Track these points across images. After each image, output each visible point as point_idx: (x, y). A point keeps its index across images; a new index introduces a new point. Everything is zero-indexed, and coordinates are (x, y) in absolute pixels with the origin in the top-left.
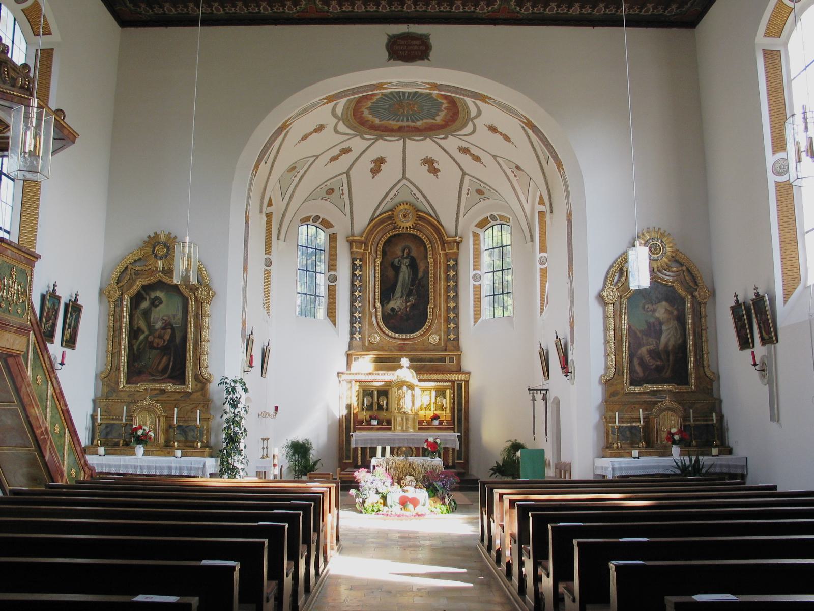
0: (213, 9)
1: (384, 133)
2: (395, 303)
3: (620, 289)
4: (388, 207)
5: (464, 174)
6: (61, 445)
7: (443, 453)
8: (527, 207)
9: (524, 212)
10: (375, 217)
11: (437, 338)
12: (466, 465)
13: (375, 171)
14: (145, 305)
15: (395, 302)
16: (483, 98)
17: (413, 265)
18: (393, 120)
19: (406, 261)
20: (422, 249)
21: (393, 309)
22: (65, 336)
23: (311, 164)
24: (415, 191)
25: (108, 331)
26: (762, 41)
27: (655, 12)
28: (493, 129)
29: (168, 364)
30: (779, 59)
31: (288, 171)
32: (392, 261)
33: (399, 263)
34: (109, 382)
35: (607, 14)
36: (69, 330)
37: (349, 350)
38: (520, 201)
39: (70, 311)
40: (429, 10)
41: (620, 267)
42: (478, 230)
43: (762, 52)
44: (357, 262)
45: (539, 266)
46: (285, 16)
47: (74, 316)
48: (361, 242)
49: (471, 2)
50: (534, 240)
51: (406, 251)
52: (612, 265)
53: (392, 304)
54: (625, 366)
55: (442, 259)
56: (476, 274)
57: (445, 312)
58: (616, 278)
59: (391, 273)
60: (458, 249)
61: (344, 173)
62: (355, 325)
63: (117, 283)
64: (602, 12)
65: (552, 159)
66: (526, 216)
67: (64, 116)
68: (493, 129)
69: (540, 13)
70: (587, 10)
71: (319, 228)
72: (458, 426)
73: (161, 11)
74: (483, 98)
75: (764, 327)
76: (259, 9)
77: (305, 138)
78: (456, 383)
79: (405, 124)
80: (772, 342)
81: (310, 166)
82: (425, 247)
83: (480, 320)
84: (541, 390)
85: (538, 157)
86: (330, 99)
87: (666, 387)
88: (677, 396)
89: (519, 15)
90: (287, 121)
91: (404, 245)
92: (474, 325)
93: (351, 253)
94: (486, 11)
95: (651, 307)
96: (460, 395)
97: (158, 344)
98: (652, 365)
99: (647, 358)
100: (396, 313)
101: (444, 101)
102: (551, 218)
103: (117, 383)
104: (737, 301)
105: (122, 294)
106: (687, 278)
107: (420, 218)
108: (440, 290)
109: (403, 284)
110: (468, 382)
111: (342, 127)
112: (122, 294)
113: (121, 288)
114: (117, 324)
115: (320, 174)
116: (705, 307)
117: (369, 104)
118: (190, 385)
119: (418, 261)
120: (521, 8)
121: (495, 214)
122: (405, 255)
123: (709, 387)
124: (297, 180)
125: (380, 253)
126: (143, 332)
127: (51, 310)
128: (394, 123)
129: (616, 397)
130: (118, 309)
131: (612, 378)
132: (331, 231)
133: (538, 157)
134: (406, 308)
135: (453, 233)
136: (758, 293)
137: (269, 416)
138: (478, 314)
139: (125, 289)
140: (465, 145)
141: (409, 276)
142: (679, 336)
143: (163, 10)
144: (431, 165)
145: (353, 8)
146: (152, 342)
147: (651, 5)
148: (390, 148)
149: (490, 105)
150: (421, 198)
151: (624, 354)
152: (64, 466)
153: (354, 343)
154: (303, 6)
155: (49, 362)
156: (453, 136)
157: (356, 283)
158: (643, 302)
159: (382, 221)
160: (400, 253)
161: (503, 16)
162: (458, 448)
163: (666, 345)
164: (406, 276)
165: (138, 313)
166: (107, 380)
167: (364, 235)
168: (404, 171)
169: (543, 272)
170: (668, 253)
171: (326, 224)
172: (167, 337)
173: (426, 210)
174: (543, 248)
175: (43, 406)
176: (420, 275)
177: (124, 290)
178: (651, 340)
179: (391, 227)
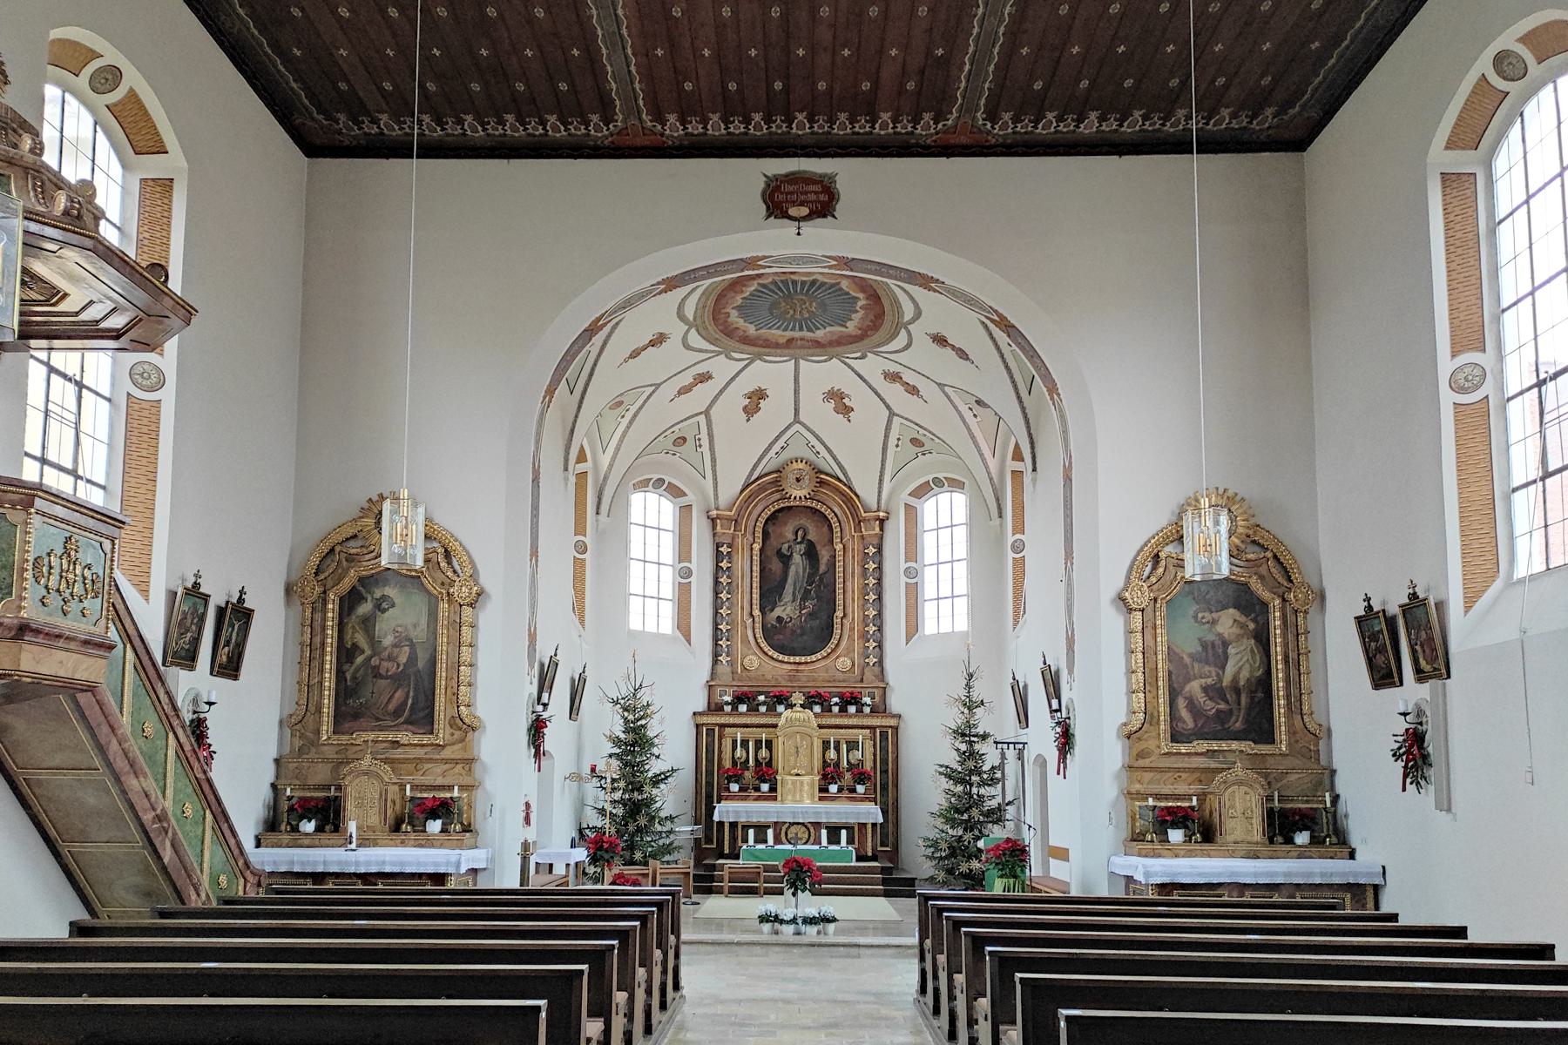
0: (466, 127)
1: (764, 350)
3: (1155, 587)
5: (892, 414)
6: (196, 836)
7: (856, 831)
8: (993, 464)
9: (989, 473)
11: (849, 663)
12: (894, 855)
13: (751, 410)
14: (365, 608)
16: (926, 282)
17: (811, 554)
18: (778, 328)
20: (825, 529)
21: (779, 619)
22: (218, 658)
23: (648, 398)
24: (814, 442)
25: (302, 651)
26: (1440, 158)
27: (1234, 125)
28: (940, 340)
29: (405, 702)
30: (1473, 189)
31: (610, 408)
34: (303, 731)
35: (1147, 131)
36: (226, 649)
37: (712, 679)
39: (227, 618)
40: (835, 131)
41: (1155, 551)
42: (912, 501)
43: (1439, 177)
44: (724, 549)
45: (1011, 555)
46: (592, 143)
47: (236, 627)
48: (729, 519)
49: (908, 115)
50: (1003, 514)
52: (1141, 550)
53: (778, 612)
54: (1161, 709)
58: (1148, 570)
59: (776, 566)
60: (882, 529)
61: (701, 413)
62: (720, 642)
63: (316, 574)
64: (1137, 128)
65: (1039, 380)
66: (991, 479)
67: (167, 277)
68: (940, 340)
69: (1026, 133)
70: (1111, 125)
72: (882, 795)
73: (375, 130)
74: (926, 282)
75: (1424, 651)
77: (635, 354)
78: (878, 731)
79: (797, 334)
80: (1439, 677)
81: (645, 402)
84: (1014, 743)
85: (1014, 382)
86: (671, 284)
87: (1235, 745)
88: (1257, 763)
89: (990, 138)
90: (598, 319)
93: (714, 535)
94: (932, 131)
95: (1208, 616)
96: (884, 749)
97: (387, 671)
98: (1210, 710)
99: (1201, 698)
100: (785, 627)
101: (861, 296)
102: (1034, 481)
103: (318, 732)
104: (1370, 607)
105: (325, 592)
106: (1273, 570)
107: (822, 483)
108: (853, 591)
109: (795, 584)
111: (695, 339)
112: (325, 592)
113: (323, 583)
114: (317, 640)
115: (666, 411)
116: (1305, 618)
117: (739, 300)
118: (443, 732)
119: (818, 548)
120: (994, 123)
121: (941, 476)
122: (799, 540)
123: (1312, 747)
124: (625, 422)
125: (759, 534)
126: (363, 652)
127: (189, 617)
128: (779, 332)
129: (1148, 761)
130: (318, 616)
131: (1140, 729)
132: (683, 501)
133: (1014, 382)
134: (800, 616)
136: (1415, 593)
139: (330, 583)
140: (894, 368)
142: (1258, 664)
143: (379, 127)
144: (838, 399)
145: (705, 128)
146: (377, 668)
147: (1228, 110)
148: (772, 373)
149: (937, 294)
150: (824, 452)
151: (1161, 692)
152: (202, 871)
153: (719, 668)
155: (167, 700)
156: (874, 353)
157: (722, 580)
158: (1195, 607)
159: (762, 489)
160: (790, 536)
161: (964, 140)
162: (881, 820)
163: (1235, 679)
164: (801, 571)
165: (353, 621)
166: (298, 726)
168: (797, 411)
169: (1020, 565)
170: (1240, 530)
171: (675, 492)
172: (403, 659)
173: (830, 471)
175: (158, 773)
176: (822, 568)
177: (329, 586)
178: (1207, 668)
179: (777, 496)
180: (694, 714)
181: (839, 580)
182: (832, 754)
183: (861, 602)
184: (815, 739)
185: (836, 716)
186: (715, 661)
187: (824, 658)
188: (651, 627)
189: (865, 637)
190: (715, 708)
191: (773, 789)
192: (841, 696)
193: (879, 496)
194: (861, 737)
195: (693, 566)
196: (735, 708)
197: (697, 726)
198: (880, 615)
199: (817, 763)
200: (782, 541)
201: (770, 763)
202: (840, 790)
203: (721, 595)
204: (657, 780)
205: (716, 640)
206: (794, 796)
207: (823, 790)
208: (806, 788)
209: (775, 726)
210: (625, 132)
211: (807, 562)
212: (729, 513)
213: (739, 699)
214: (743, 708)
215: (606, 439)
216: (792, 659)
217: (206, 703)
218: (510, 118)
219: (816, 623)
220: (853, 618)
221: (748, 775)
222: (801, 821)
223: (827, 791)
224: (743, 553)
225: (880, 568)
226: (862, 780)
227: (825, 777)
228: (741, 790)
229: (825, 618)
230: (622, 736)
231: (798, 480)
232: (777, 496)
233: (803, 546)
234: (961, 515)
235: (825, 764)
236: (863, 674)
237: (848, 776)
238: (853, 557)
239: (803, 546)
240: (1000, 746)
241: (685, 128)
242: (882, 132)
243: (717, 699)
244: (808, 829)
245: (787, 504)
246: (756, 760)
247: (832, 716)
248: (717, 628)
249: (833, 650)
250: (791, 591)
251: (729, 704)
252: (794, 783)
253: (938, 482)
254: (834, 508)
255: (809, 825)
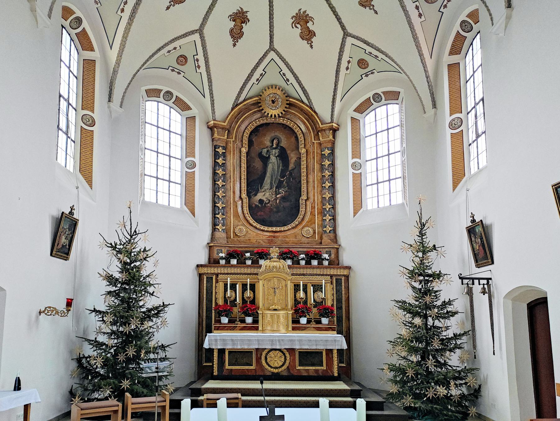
2: (264, 195)
4: (256, 90)
9: (426, 71)
10: (239, 102)
15: (264, 193)
17: (283, 156)
19: (276, 152)
20: (293, 139)
21: (261, 201)
24: (285, 70)
32: (260, 151)
33: (267, 154)
38: (421, 55)
42: (357, 115)
44: (220, 150)
48: (223, 128)
51: (275, 141)
53: (260, 196)
55: (316, 150)
56: (355, 162)
57: (319, 204)
59: (258, 164)
60: (334, 137)
71: (173, 108)
78: (334, 278)
82: (297, 137)
83: (361, 210)
84: (479, 279)
91: (273, 135)
92: (354, 216)
93: (213, 140)
96: (338, 292)
100: (265, 206)
107: (291, 105)
108: (314, 182)
109: (272, 177)
110: (348, 277)
119: (288, 152)
122: (274, 146)
134: (276, 199)
135: (328, 119)
137: (57, 313)
138: (358, 204)
141: (278, 167)
150: (292, 80)
153: (218, 234)
159: (247, 109)
160: (268, 143)
162: (345, 347)
167: (227, 121)
171: (182, 105)
176: (291, 166)
180: (198, 266)
181: (304, 174)
182: (301, 294)
183: (320, 189)
184: (289, 282)
185: (303, 267)
186: (214, 229)
187: (293, 228)
188: (163, 200)
189: (322, 213)
190: (213, 262)
191: (256, 321)
192: (307, 254)
193: (333, 111)
194: (324, 281)
195: (197, 160)
196: (228, 262)
197: (200, 276)
198: (333, 197)
199: (290, 302)
200: (262, 147)
201: (253, 302)
202: (309, 322)
203: (218, 183)
204: (150, 314)
205: (214, 214)
206: (272, 326)
207: (296, 321)
208: (282, 319)
209: (257, 274)
211: (280, 162)
212: (223, 124)
213: (230, 255)
214: (234, 262)
215: (111, 35)
216: (270, 229)
219: (287, 204)
220: (314, 200)
221: (236, 310)
222: (278, 348)
223: (298, 322)
224: (234, 154)
225: (333, 165)
226: (326, 313)
227: (296, 311)
228: (230, 322)
229: (293, 200)
230: (117, 275)
231: (273, 102)
232: (259, 115)
233: (277, 151)
234: (395, 120)
235: (296, 302)
236: (321, 238)
237: (315, 310)
238: (314, 158)
239: (277, 151)
240: (465, 281)
243: (215, 256)
244: (284, 354)
245: (265, 121)
246: (243, 298)
247: (300, 268)
248: (215, 206)
249: (300, 223)
250: (269, 181)
251: (223, 259)
252: (272, 316)
253: (377, 98)
254: (301, 126)
255: (285, 351)
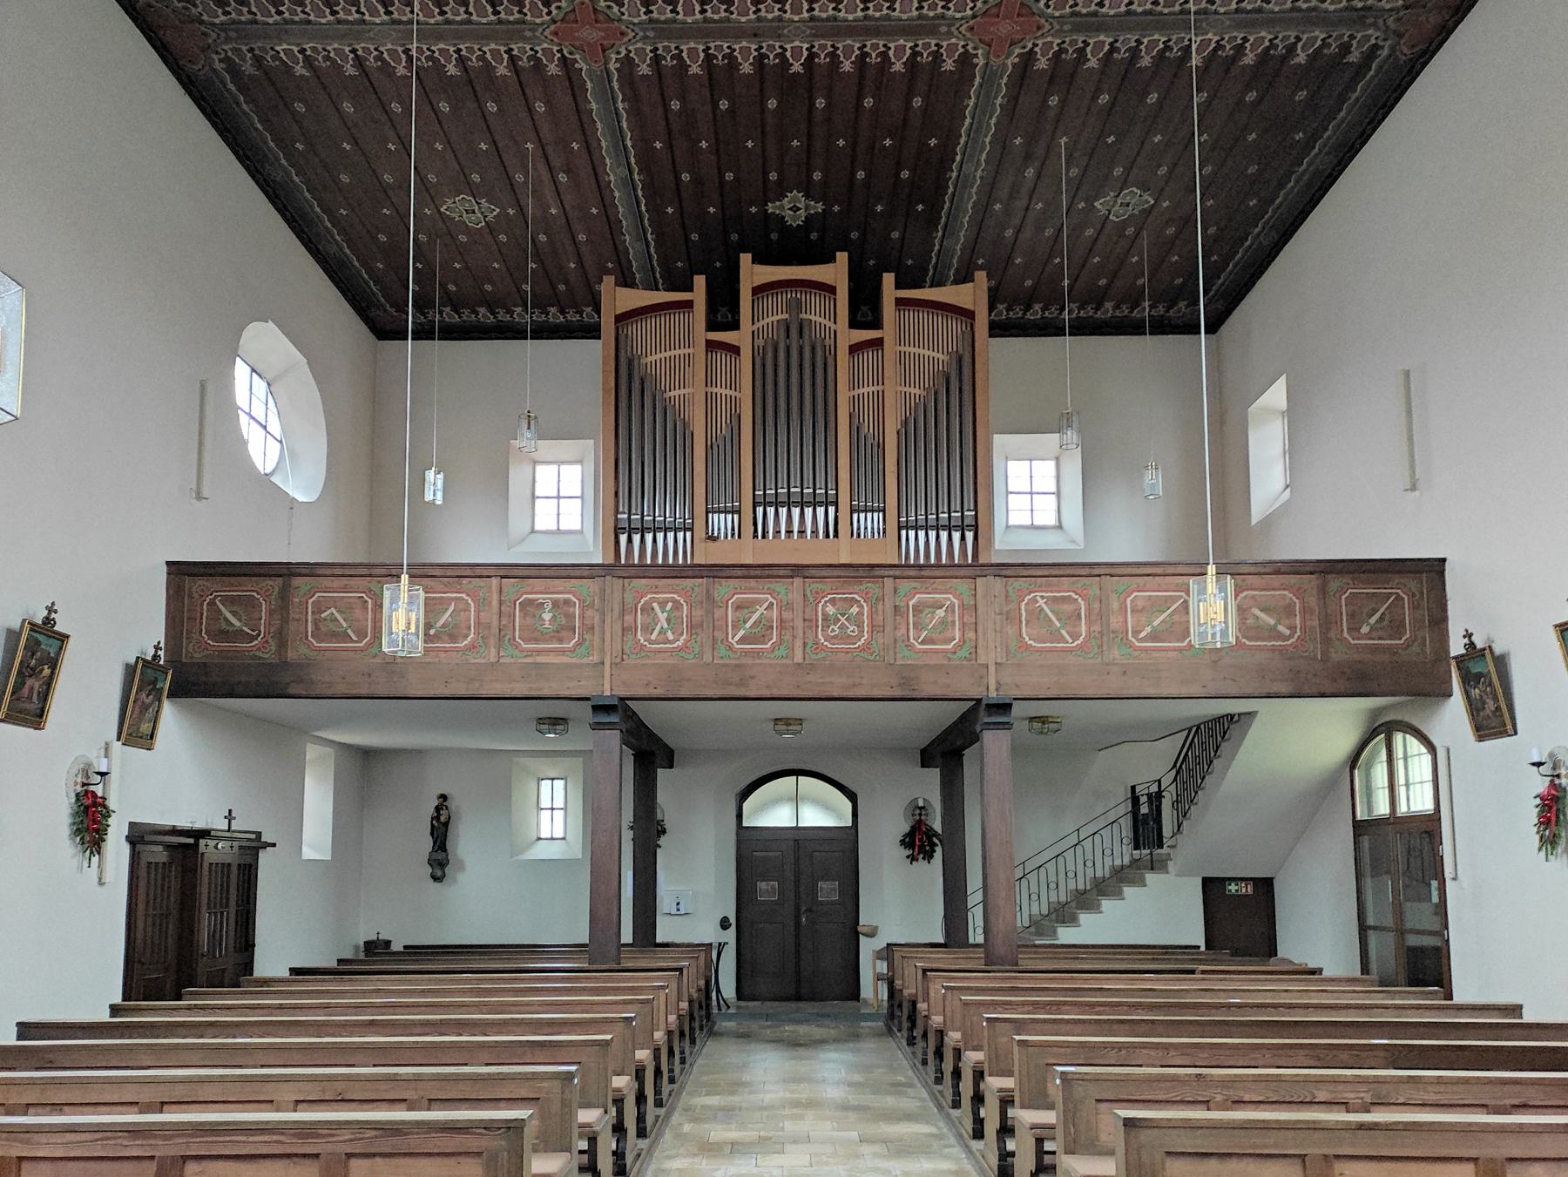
27: (1118, 313)
73: (508, 317)
76: (581, 316)
104: (1471, 645)
154: (614, 56)
174: (835, 323)
210: (572, 17)
217: (98, 773)
218: (553, 310)
241: (649, 12)
242: (902, 42)
